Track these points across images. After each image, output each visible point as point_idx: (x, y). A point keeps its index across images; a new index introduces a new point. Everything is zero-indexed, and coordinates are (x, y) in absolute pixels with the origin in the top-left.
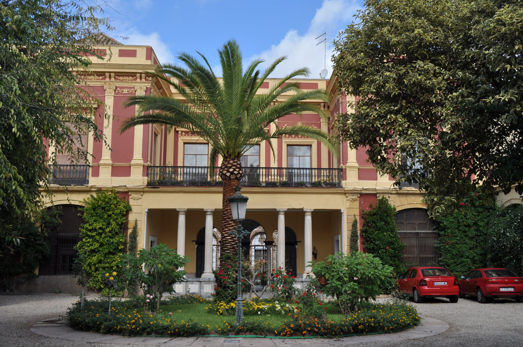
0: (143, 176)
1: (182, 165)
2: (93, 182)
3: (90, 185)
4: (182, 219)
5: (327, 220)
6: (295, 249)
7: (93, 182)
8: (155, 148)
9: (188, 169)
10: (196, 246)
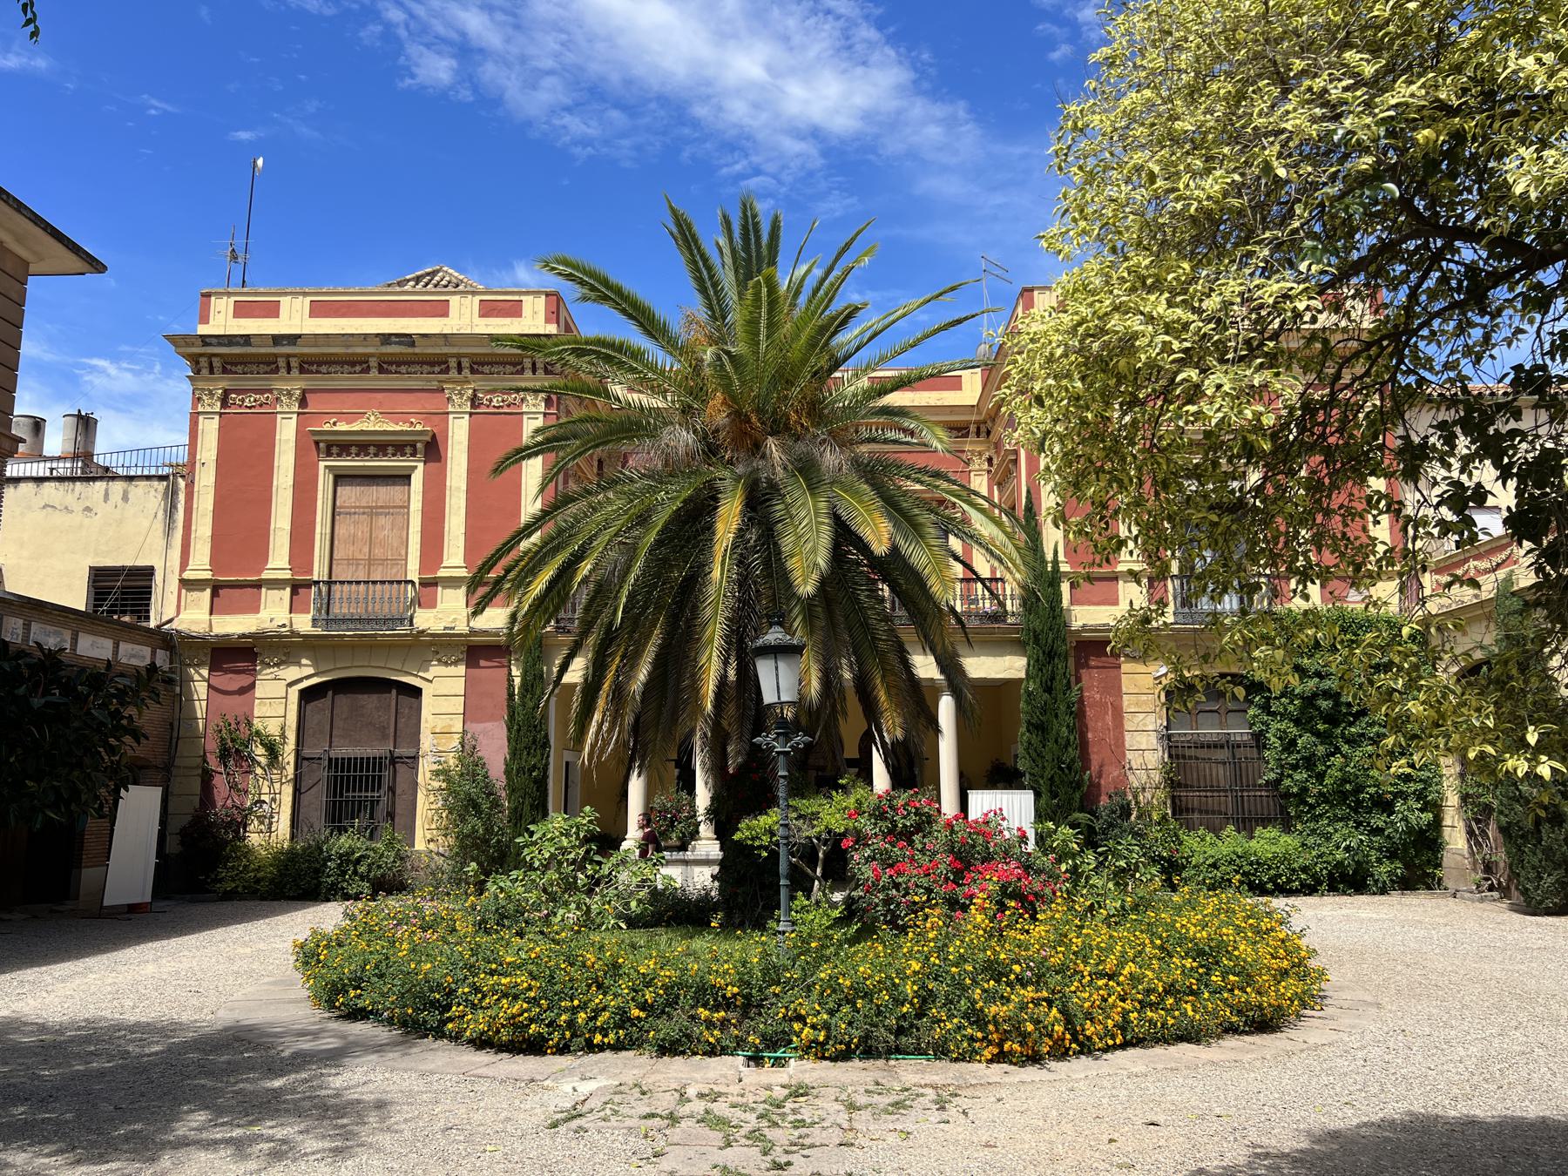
10: (676, 772)
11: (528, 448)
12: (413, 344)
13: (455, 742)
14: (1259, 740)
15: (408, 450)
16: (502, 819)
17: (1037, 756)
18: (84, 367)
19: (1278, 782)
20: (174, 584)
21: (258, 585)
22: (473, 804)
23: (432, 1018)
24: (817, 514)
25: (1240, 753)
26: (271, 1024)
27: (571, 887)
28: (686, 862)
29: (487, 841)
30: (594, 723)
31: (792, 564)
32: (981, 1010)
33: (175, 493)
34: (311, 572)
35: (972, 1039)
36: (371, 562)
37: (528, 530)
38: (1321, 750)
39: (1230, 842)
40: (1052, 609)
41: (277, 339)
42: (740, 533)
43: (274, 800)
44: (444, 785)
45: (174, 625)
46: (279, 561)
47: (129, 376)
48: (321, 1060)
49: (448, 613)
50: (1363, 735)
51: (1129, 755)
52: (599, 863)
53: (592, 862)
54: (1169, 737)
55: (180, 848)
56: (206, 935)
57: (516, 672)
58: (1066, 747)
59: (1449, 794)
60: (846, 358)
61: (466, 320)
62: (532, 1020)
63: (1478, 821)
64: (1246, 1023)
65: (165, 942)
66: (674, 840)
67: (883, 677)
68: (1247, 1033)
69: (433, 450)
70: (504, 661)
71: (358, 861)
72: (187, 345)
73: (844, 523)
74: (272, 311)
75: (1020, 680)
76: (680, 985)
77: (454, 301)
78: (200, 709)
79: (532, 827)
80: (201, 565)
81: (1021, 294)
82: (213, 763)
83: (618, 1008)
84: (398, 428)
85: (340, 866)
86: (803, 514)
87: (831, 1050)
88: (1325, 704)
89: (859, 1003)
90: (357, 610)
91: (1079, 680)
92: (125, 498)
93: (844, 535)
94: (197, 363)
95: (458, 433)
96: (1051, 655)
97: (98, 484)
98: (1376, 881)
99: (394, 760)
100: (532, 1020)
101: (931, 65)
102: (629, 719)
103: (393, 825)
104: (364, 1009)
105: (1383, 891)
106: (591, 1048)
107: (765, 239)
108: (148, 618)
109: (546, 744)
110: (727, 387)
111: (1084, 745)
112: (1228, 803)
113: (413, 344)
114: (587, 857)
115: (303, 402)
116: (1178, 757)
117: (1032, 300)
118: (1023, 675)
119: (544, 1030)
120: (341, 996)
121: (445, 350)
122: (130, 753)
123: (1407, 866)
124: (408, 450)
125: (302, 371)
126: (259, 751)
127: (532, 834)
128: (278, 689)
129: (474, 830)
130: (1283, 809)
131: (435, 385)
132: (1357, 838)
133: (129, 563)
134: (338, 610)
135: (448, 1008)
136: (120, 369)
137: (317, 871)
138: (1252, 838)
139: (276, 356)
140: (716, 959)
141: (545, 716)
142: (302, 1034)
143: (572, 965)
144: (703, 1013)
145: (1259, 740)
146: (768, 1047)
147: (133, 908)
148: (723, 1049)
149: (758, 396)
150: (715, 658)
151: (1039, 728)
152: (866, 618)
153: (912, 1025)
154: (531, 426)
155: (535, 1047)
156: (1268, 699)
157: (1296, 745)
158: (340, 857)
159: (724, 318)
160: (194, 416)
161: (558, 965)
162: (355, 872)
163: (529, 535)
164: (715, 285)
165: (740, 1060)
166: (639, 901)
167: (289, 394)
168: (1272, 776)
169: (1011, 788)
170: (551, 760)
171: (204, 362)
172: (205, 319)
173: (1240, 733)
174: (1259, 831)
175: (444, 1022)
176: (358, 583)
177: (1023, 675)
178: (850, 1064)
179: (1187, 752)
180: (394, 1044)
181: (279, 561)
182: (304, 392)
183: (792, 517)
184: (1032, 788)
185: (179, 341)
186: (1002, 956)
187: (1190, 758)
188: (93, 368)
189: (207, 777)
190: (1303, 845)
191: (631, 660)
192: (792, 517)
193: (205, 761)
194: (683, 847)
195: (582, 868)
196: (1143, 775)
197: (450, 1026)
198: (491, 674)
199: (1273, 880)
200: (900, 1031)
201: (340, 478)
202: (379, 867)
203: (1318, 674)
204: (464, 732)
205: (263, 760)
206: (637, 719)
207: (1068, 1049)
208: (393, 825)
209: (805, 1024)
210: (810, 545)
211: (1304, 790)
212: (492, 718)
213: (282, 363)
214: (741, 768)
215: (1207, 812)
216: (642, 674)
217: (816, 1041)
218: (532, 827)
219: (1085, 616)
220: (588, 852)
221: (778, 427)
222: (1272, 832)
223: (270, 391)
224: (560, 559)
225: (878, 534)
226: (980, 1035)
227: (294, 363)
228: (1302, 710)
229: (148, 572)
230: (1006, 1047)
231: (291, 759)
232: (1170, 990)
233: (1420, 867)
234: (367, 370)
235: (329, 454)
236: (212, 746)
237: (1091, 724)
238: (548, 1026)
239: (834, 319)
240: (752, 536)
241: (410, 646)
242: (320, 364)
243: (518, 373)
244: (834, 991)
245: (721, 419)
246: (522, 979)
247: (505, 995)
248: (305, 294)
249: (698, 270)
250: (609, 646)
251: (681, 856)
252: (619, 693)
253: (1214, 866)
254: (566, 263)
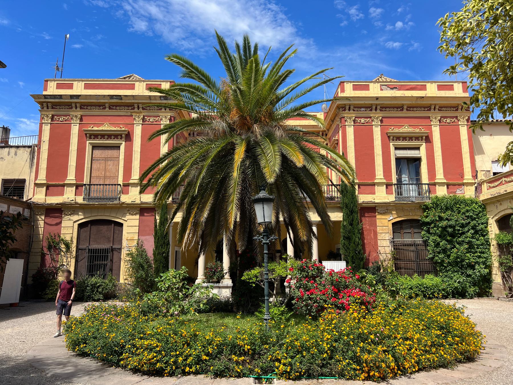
11: (163, 130)
12: (121, 99)
13: (135, 243)
14: (426, 243)
15: (119, 137)
16: (152, 271)
17: (347, 249)
18: (18, 121)
19: (433, 258)
20: (32, 185)
21: (63, 186)
22: (141, 266)
23: (115, 359)
24: (274, 152)
25: (420, 247)
26: (48, 359)
27: (177, 298)
28: (219, 287)
29: (146, 280)
30: (186, 235)
31: (265, 171)
32: (359, 356)
33: (34, 152)
34: (83, 181)
35: (355, 369)
36: (105, 177)
37: (161, 160)
38: (449, 246)
39: (416, 280)
40: (352, 195)
41: (72, 97)
42: (243, 161)
43: (68, 264)
44: (131, 259)
45: (32, 200)
46: (71, 177)
47: (33, 124)
48: (62, 379)
49: (133, 196)
50: (463, 241)
51: (380, 248)
52: (188, 289)
53: (185, 288)
54: (394, 242)
55: (32, 282)
56: (36, 316)
57: (158, 218)
58: (358, 245)
59: (494, 262)
60: (282, 98)
61: (141, 91)
62: (158, 361)
63: (506, 272)
64: (464, 359)
65: (19, 319)
66: (215, 279)
67: (299, 216)
68: (464, 363)
69: (128, 137)
70: (153, 214)
71: (99, 287)
72: (39, 98)
73: (285, 155)
74: (70, 87)
75: (341, 221)
76: (223, 345)
77: (137, 84)
78: (41, 231)
79: (162, 275)
80: (42, 178)
81: (340, 84)
82: (46, 251)
83: (197, 355)
84: (116, 129)
85: (91, 289)
86: (269, 152)
87: (293, 375)
88: (450, 230)
89: (304, 353)
90: (100, 195)
91: (361, 222)
92: (16, 154)
93: (285, 160)
94: (43, 105)
95: (138, 131)
96: (352, 212)
97: (6, 149)
98: (469, 294)
99: (113, 250)
100: (158, 361)
102: (200, 232)
103: (112, 273)
104: (86, 353)
105: (472, 298)
106: (184, 373)
107: (252, 52)
108: (23, 198)
109: (168, 244)
110: (238, 104)
111: (363, 245)
112: (414, 266)
113: (121, 99)
114: (183, 286)
115: (81, 120)
116: (397, 249)
117: (344, 86)
118: (342, 219)
119: (163, 366)
120: (79, 346)
121: (133, 101)
122: (10, 247)
123: (480, 288)
124: (119, 137)
125: (81, 108)
126: (63, 246)
127: (161, 277)
128: (70, 223)
129: (142, 276)
130: (435, 267)
131: (129, 114)
132: (462, 279)
133: (17, 178)
134: (92, 195)
135: (121, 354)
136: (31, 122)
137: (83, 291)
138: (423, 278)
139: (71, 103)
140: (239, 333)
141: (167, 233)
142: (59, 364)
143: (176, 335)
144: (235, 358)
145: (426, 243)
146: (264, 373)
147: (12, 305)
148: (244, 374)
149: (249, 110)
150: (234, 208)
151: (348, 238)
152: (292, 194)
153: (327, 363)
154: (165, 122)
155: (159, 373)
156: (429, 228)
157: (440, 244)
158: (92, 285)
159: (237, 81)
160: (41, 125)
161: (170, 335)
162: (97, 291)
163: (162, 163)
164: (234, 68)
165: (251, 380)
166: (204, 304)
167: (76, 117)
168: (431, 256)
169: (336, 260)
170: (170, 250)
171: (45, 104)
172: (46, 90)
173: (419, 240)
174: (426, 276)
175: (119, 361)
177: (342, 219)
178: (301, 382)
179: (400, 247)
180: (98, 370)
181: (71, 177)
182: (82, 116)
183: (264, 154)
184: (345, 260)
185: (35, 97)
186: (366, 331)
187: (401, 249)
188: (22, 122)
189: (43, 255)
190: (443, 281)
191: (201, 210)
192: (264, 154)
193: (42, 250)
194: (218, 282)
195: (181, 291)
196: (384, 255)
197: (122, 362)
198: (148, 218)
199: (432, 294)
200: (323, 366)
201: (95, 147)
202: (106, 289)
203: (447, 219)
204: (139, 239)
205: (64, 250)
206: (203, 232)
207: (396, 374)
208: (112, 273)
209: (280, 363)
210: (272, 163)
211: (443, 261)
212: (149, 235)
213: (73, 105)
214: (244, 252)
215: (407, 269)
216: (206, 214)
217: (286, 371)
218: (162, 275)
219: (363, 198)
220: (183, 284)
221: (257, 120)
222: (431, 276)
223: (69, 115)
224: (173, 170)
225: (299, 160)
226: (358, 368)
227: (78, 105)
228: (442, 232)
229: (23, 181)
230: (371, 374)
231: (75, 249)
232: (433, 345)
233: (484, 289)
234: (105, 108)
235: (90, 138)
236: (45, 244)
237: (366, 237)
238: (165, 363)
239: (280, 77)
240: (248, 163)
241: (119, 208)
242: (87, 106)
244: (292, 347)
245: (236, 118)
246: (154, 342)
247: (147, 349)
248: (83, 81)
249: (227, 62)
250: (192, 205)
251: (217, 285)
252: (196, 224)
253: (411, 288)
254: (177, 58)
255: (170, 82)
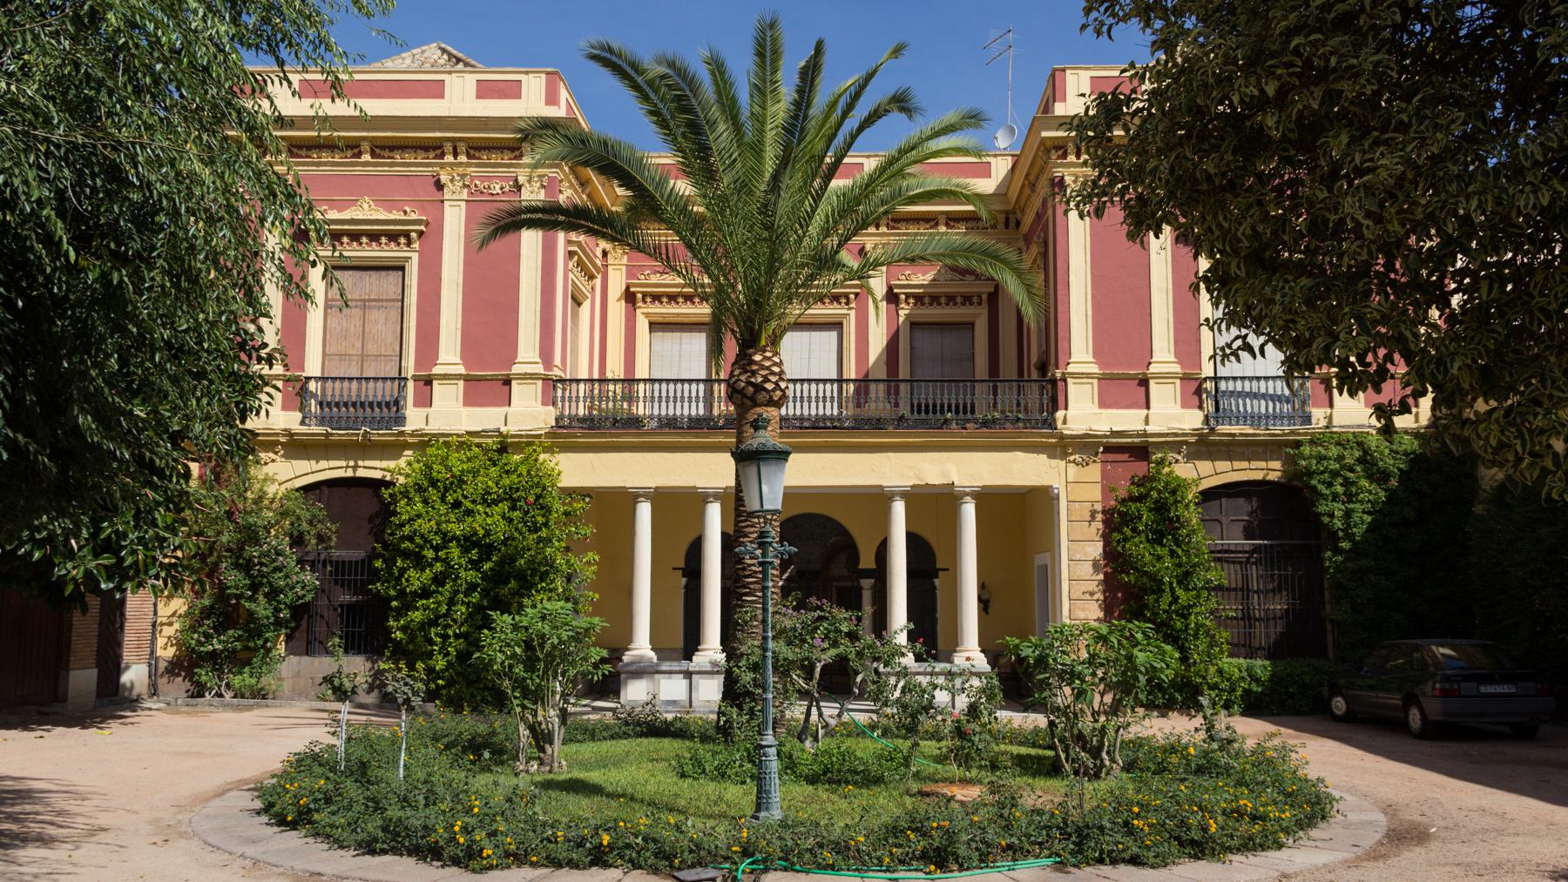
0: (544, 403)
1: (586, 376)
2: (415, 419)
3: (408, 428)
4: (969, 511)
5: (1018, 518)
6: (934, 588)
7: (415, 419)
8: (576, 335)
9: (1271, 383)
10: (684, 580)
15: (402, 240)
69: (430, 234)
84: (392, 217)
101: (1284, 243)
176: (351, 379)
201: (655, 326)
213: (448, 147)
243: (515, 158)
255: (547, 73)
